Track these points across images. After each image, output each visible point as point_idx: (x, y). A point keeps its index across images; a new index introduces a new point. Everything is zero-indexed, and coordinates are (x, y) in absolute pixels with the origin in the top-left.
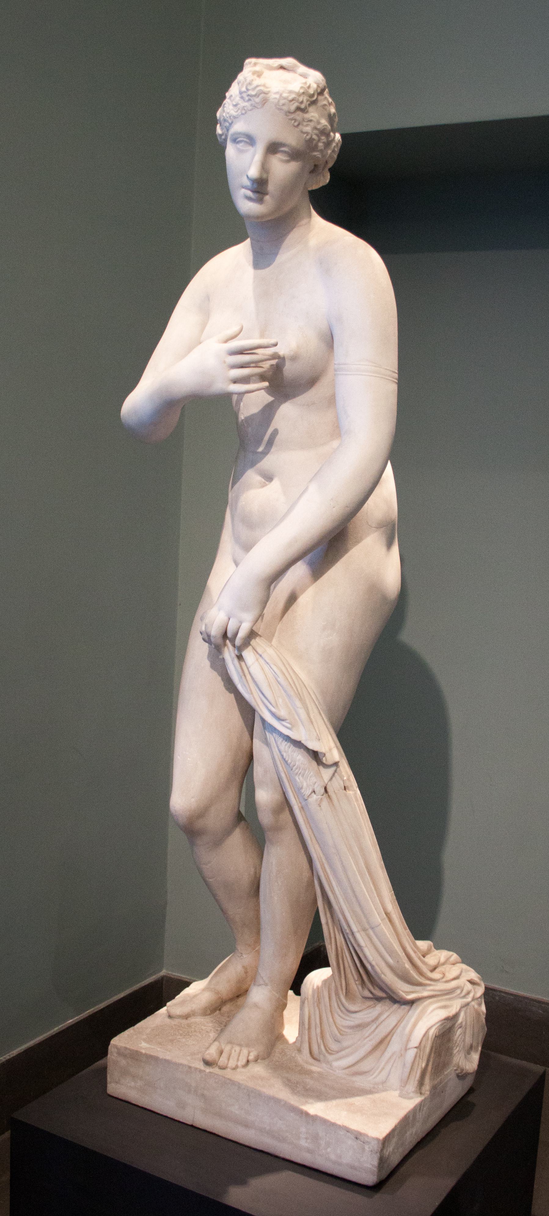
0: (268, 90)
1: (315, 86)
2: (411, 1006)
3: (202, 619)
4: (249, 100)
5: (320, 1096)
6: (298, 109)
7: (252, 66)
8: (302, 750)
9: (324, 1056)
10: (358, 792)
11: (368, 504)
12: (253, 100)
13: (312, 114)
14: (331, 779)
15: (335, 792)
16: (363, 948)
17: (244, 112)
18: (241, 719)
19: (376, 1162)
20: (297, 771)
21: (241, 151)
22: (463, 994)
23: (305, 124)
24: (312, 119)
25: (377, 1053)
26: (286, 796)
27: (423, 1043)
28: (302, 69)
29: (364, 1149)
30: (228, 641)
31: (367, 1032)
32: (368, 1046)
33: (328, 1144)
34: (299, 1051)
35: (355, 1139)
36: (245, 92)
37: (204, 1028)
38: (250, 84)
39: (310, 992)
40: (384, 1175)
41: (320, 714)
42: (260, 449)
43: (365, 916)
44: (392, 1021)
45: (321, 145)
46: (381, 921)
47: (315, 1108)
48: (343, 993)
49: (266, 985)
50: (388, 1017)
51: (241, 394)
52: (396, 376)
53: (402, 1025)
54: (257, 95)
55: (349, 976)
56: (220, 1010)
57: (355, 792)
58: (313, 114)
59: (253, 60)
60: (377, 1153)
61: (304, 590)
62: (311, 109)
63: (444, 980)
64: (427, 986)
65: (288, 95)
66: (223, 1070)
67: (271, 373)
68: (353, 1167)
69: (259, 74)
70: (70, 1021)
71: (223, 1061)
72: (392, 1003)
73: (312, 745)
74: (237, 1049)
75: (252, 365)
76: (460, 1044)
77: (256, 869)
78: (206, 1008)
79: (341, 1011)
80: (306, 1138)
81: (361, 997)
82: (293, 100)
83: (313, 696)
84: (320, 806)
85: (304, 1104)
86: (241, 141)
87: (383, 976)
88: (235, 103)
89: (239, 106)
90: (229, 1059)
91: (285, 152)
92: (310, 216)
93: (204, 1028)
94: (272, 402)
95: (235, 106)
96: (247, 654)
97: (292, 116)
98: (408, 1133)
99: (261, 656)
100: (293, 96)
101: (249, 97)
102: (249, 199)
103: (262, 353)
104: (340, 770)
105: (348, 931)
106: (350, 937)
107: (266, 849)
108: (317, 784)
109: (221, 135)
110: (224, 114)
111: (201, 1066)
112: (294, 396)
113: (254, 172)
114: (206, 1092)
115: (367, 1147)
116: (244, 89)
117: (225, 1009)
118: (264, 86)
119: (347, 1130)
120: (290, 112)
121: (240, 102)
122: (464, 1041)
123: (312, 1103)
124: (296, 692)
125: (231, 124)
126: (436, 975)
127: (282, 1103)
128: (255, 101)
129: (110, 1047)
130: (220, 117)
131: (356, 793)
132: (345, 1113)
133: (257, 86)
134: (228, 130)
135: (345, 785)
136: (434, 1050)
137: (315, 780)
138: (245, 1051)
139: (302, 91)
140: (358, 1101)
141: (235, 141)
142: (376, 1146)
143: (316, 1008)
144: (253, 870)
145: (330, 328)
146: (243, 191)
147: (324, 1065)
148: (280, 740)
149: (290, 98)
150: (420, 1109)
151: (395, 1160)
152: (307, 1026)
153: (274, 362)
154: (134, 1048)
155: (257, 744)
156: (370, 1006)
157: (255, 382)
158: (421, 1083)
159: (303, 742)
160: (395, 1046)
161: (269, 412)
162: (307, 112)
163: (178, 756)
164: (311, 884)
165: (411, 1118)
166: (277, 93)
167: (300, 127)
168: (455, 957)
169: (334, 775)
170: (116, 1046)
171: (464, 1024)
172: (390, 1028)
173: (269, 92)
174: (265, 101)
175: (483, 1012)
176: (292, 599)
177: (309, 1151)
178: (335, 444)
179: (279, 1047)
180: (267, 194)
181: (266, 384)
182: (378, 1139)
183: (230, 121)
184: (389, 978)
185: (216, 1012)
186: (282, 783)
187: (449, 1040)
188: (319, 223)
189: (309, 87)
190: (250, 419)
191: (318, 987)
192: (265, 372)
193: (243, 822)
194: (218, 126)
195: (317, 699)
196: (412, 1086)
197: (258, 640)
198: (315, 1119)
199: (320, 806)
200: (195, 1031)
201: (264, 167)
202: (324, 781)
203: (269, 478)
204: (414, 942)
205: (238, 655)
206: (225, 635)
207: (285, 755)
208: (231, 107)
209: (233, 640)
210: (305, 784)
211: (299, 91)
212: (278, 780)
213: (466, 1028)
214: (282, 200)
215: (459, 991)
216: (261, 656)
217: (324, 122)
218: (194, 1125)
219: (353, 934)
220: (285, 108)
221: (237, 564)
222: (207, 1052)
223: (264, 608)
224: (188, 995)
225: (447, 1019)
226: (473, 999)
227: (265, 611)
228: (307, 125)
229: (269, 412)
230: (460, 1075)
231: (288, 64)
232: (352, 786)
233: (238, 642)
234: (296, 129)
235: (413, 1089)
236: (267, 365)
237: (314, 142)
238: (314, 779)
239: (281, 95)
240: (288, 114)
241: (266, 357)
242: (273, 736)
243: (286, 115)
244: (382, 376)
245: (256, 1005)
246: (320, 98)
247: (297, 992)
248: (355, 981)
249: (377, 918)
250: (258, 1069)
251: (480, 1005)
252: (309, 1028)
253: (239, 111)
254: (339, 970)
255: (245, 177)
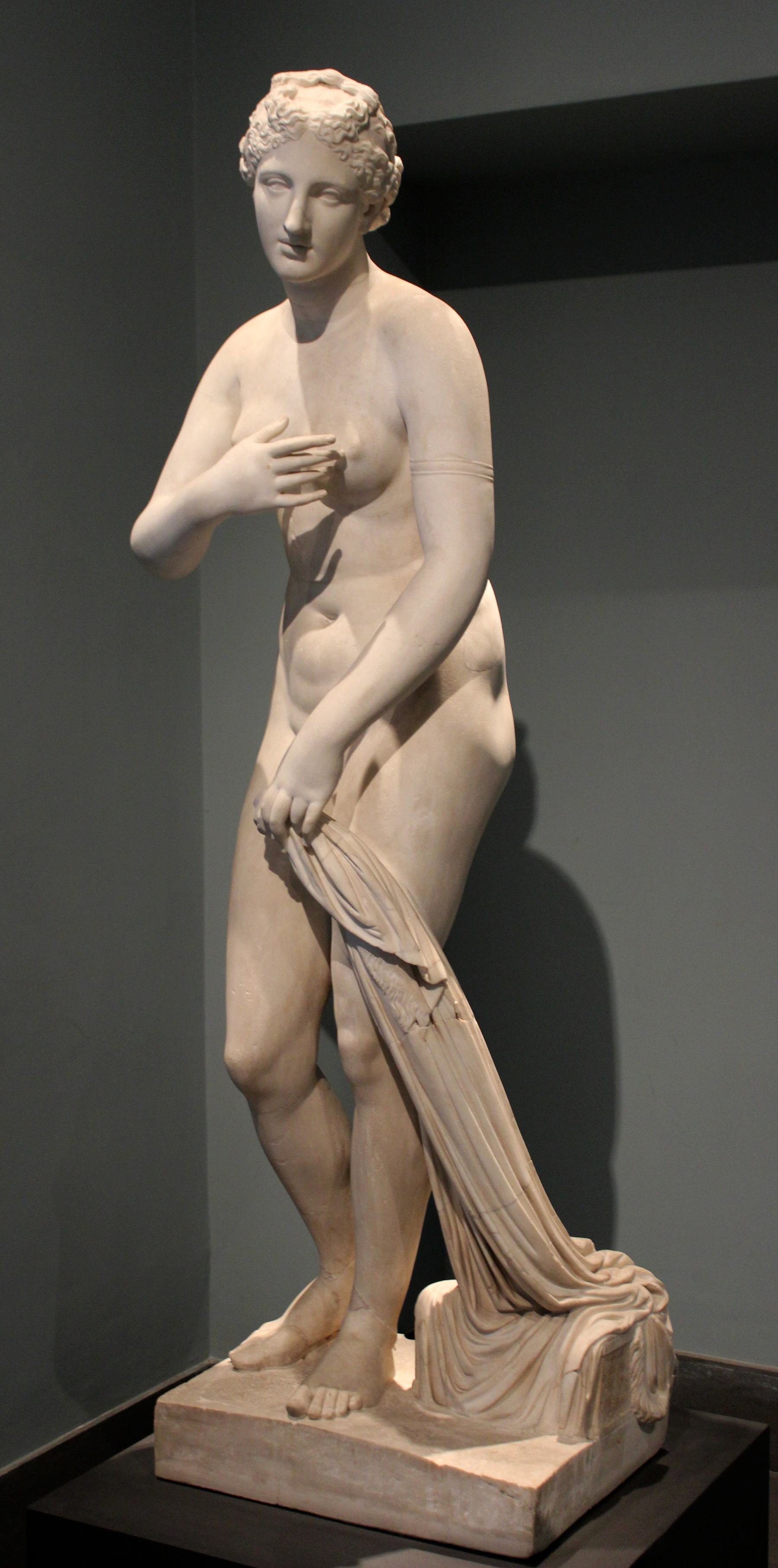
0: (305, 116)
1: (364, 105)
2: (566, 1317)
3: (256, 803)
4: (282, 130)
5: (450, 1444)
6: (346, 138)
7: (283, 85)
8: (397, 966)
9: (453, 1396)
10: (475, 1023)
11: (464, 640)
12: (287, 129)
13: (364, 142)
14: (437, 1005)
15: (443, 1021)
16: (494, 1235)
17: (275, 145)
18: (313, 936)
19: (530, 1524)
20: (392, 995)
21: (273, 195)
22: (638, 1302)
23: (355, 155)
24: (364, 148)
25: (524, 1387)
26: (380, 1031)
27: (586, 1364)
28: (349, 83)
29: (513, 1506)
30: (292, 829)
31: (510, 1355)
32: (511, 1374)
33: (465, 1507)
34: (418, 1397)
35: (501, 1494)
36: (276, 120)
37: (283, 1379)
38: (282, 109)
39: (428, 1312)
40: (544, 1545)
41: (418, 917)
42: (319, 577)
43: (496, 1192)
44: (541, 1339)
45: (376, 179)
46: (517, 1196)
47: (442, 1458)
48: (472, 1305)
49: (367, 1307)
50: (536, 1332)
51: (289, 508)
52: (491, 472)
53: (555, 1343)
54: (292, 124)
55: (480, 1284)
56: (304, 1358)
57: (471, 1023)
58: (365, 142)
59: (282, 76)
60: (530, 1509)
61: (387, 758)
62: (361, 136)
63: (610, 1282)
64: (584, 1289)
65: (332, 120)
66: (315, 1421)
67: (328, 478)
68: (499, 1534)
69: (292, 95)
70: (81, 1428)
71: (313, 1408)
72: (540, 1316)
73: (410, 958)
74: (333, 1392)
75: (302, 469)
76: (638, 1374)
77: (343, 1146)
78: (285, 1353)
79: (472, 1333)
80: (435, 1502)
81: (496, 1311)
82: (338, 127)
83: (408, 896)
84: (425, 1041)
85: (428, 1454)
86: (274, 183)
87: (524, 1273)
88: (263, 134)
89: (269, 138)
90: (322, 1406)
91: (330, 194)
92: (366, 269)
93: (283, 1379)
94: (332, 515)
95: (263, 137)
96: (319, 844)
97: (338, 148)
98: (573, 1492)
99: (336, 845)
100: (338, 122)
101: (283, 127)
102: (290, 257)
103: (316, 453)
104: (449, 992)
105: (473, 1213)
106: (477, 1221)
107: (356, 1114)
108: (419, 1011)
109: (245, 174)
110: (250, 147)
111: (285, 1418)
112: (360, 506)
113: (292, 222)
114: (293, 1454)
115: (517, 1503)
116: (274, 116)
117: (312, 1356)
118: (300, 111)
119: (489, 1482)
120: (335, 143)
121: (270, 133)
122: (644, 1369)
123: (439, 1453)
124: (385, 888)
125: (259, 161)
126: (599, 1276)
127: (399, 1455)
128: (289, 131)
129: (157, 1408)
130: (244, 150)
131: (471, 1024)
132: (485, 1462)
133: (292, 112)
134: (256, 167)
135: (457, 1012)
136: (601, 1375)
137: (416, 1006)
138: (344, 1395)
139: (349, 115)
140: (501, 1448)
141: (265, 182)
142: (528, 1500)
143: (438, 1332)
144: (338, 1146)
145: (401, 412)
146: (280, 245)
147: (453, 1410)
148: (367, 955)
149: (335, 125)
150: (587, 1460)
151: (559, 1526)
152: (426, 1360)
153: (332, 463)
154: (191, 1404)
155: (338, 968)
156: (510, 1322)
157: (308, 491)
158: (587, 1424)
159: (398, 954)
160: (547, 1373)
161: (328, 528)
162: (358, 140)
163: (233, 992)
164: (419, 1158)
165: (576, 1469)
166: (317, 120)
167: (350, 160)
168: (625, 1257)
169: (440, 999)
170: (165, 1406)
171: (642, 1344)
172: (540, 1347)
173: (307, 119)
174: (302, 131)
175: (668, 1332)
176: (373, 770)
177: (439, 1519)
178: (417, 564)
179: (389, 1394)
180: (311, 248)
181: (323, 492)
182: (530, 1490)
183: (258, 157)
184: (533, 1276)
185: (298, 1360)
186: (370, 1009)
187: (623, 1366)
188: (377, 275)
189: (358, 108)
190: (303, 539)
191: (438, 1304)
192: (321, 477)
193: (322, 1080)
194: (242, 160)
195: (412, 897)
196: (574, 1426)
197: (331, 824)
198: (445, 1471)
199: (425, 1041)
200: (272, 1383)
201: (306, 215)
202: (428, 1007)
203: (332, 615)
204: (571, 1241)
205: (306, 845)
206: (288, 822)
207: (374, 974)
208: (258, 138)
209: (298, 827)
210: (403, 1012)
211: (345, 115)
212: (369, 1019)
213: (645, 1353)
214: (330, 255)
215: (631, 1299)
216: (336, 845)
217: (379, 151)
218: (280, 1504)
219: (480, 1217)
220: (328, 138)
221: (296, 731)
222: (294, 1398)
223: (336, 783)
224: (259, 1339)
225: (616, 1333)
226: (652, 1311)
227: (338, 790)
228: (357, 158)
229: (328, 528)
230: (642, 1420)
231: (329, 78)
232: (466, 1013)
233: (306, 828)
234: (345, 164)
235: (577, 1431)
236: (322, 469)
237: (368, 178)
238: (415, 1005)
239: (322, 123)
240: (333, 146)
241: (321, 458)
242: (358, 951)
243: (330, 147)
244: (473, 474)
245: (354, 1337)
246: (373, 119)
247: (410, 1336)
248: (487, 1288)
249: (513, 1192)
250: (362, 1418)
251: (664, 1320)
252: (430, 1363)
253: (270, 144)
254: (467, 1279)
255: (282, 229)
